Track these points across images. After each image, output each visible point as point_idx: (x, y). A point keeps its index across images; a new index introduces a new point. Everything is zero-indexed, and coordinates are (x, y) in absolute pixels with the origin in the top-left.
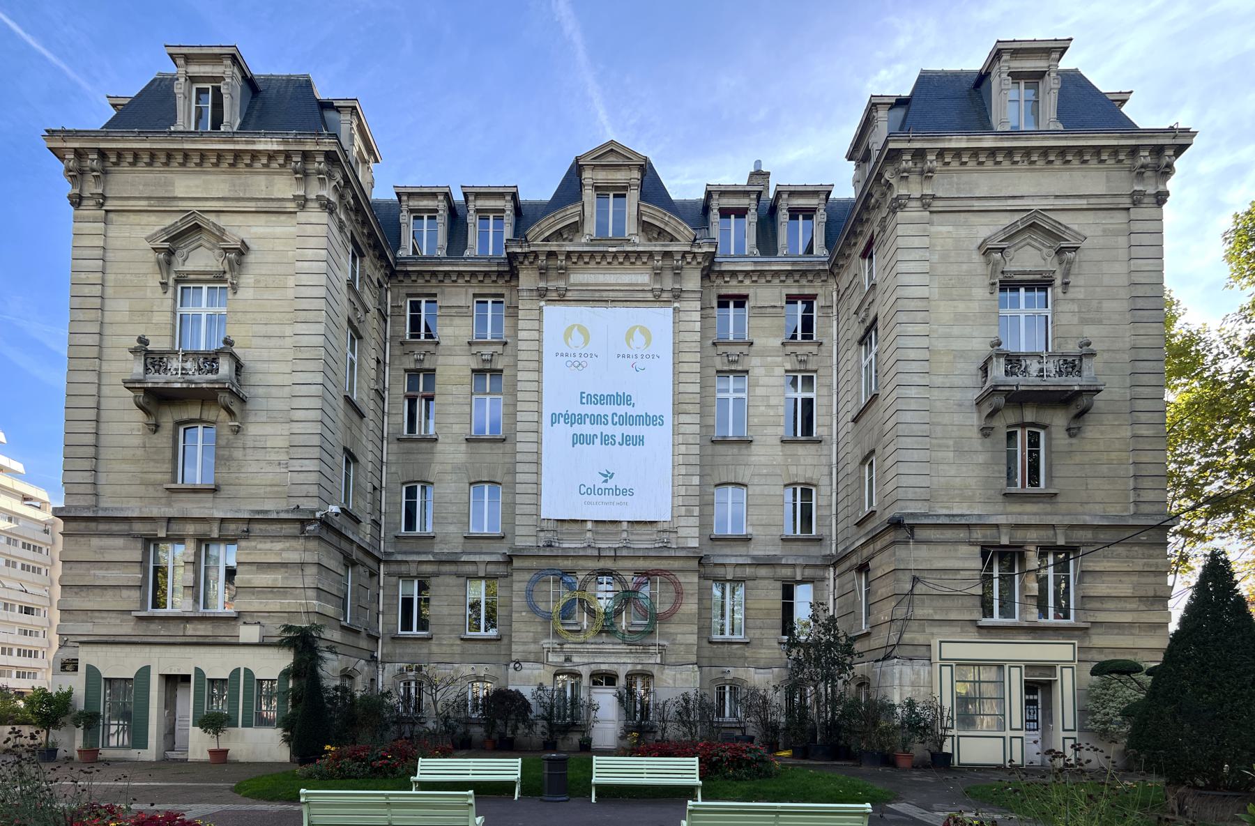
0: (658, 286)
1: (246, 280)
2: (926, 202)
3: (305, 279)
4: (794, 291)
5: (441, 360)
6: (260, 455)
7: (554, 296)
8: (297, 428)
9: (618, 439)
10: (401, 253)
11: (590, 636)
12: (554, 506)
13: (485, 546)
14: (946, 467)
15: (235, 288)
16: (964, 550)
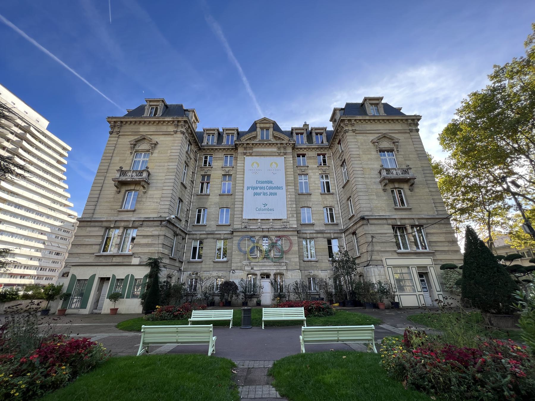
1: (156, 151)
4: (319, 153)
5: (213, 172)
8: (164, 192)
11: (260, 260)
13: (224, 228)
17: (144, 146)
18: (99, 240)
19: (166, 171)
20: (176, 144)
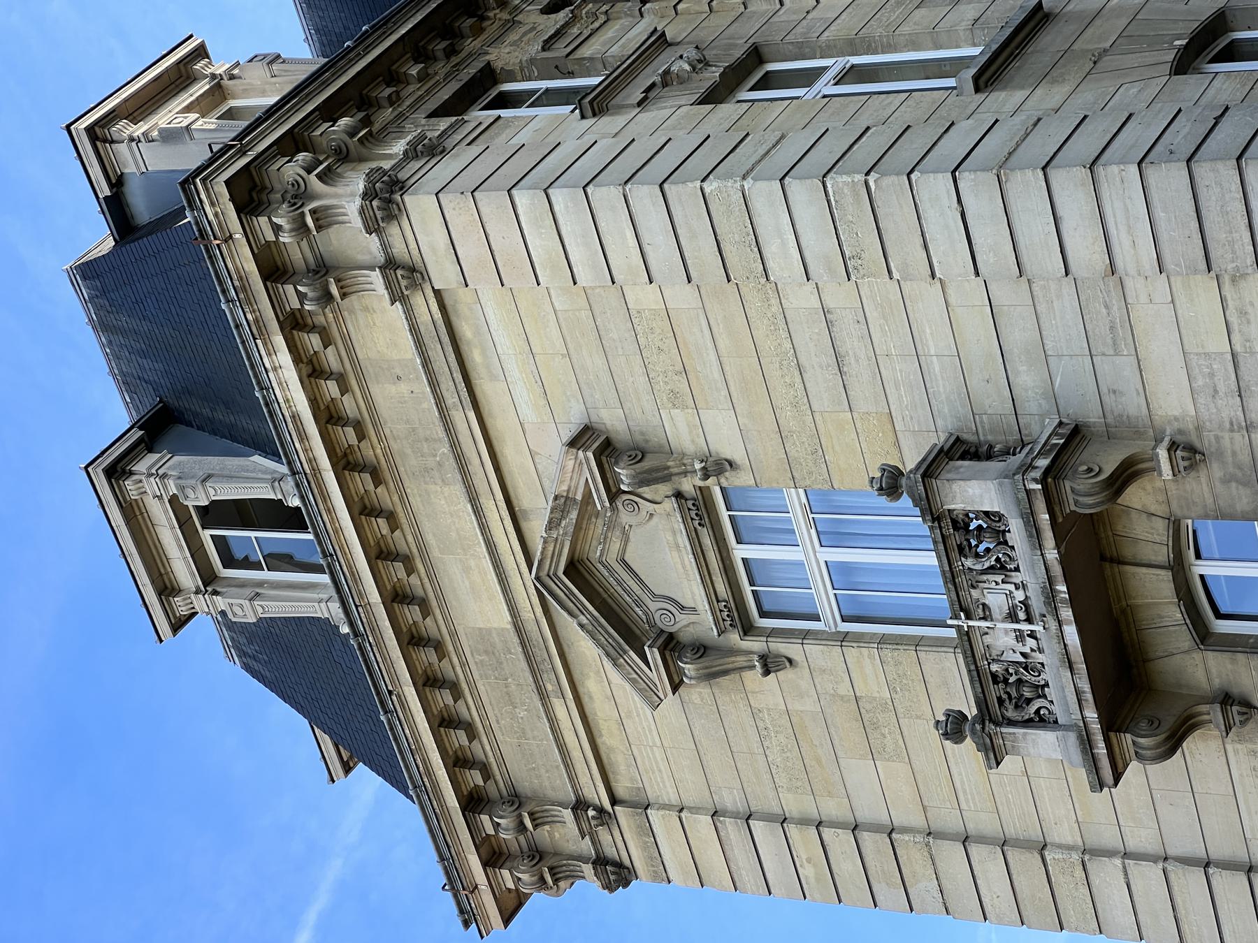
1: (680, 431)
8: (1134, 251)
19: (877, 288)
20: (542, 244)
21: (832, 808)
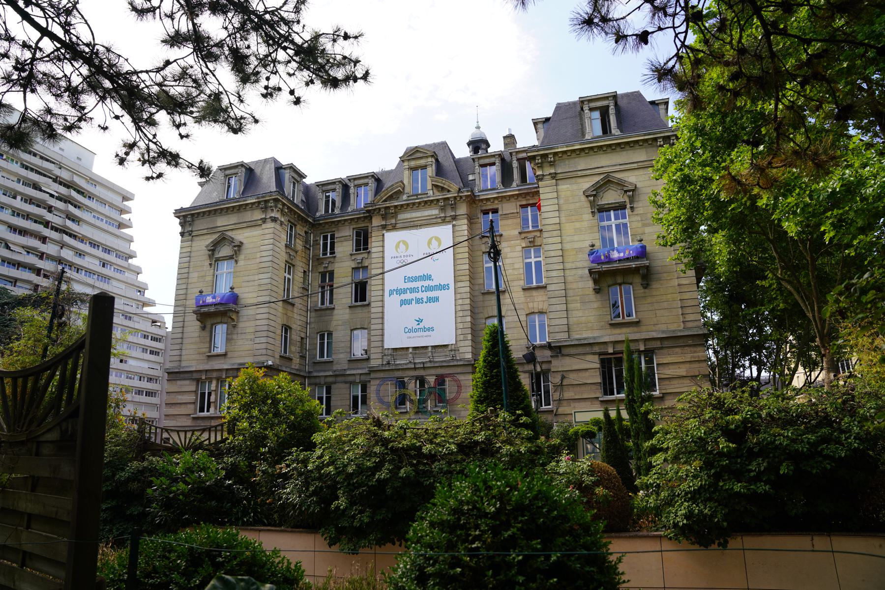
0: (443, 215)
1: (241, 257)
2: (554, 176)
3: (264, 254)
4: (524, 203)
5: (336, 265)
6: (243, 336)
7: (390, 227)
8: (258, 323)
9: (425, 300)
10: (318, 214)
11: (412, 414)
12: (392, 341)
13: (359, 365)
14: (577, 312)
15: (236, 262)
16: (589, 357)
17: (225, 251)
18: (191, 398)
19: (256, 289)
20: (266, 242)
21: (191, 270)
